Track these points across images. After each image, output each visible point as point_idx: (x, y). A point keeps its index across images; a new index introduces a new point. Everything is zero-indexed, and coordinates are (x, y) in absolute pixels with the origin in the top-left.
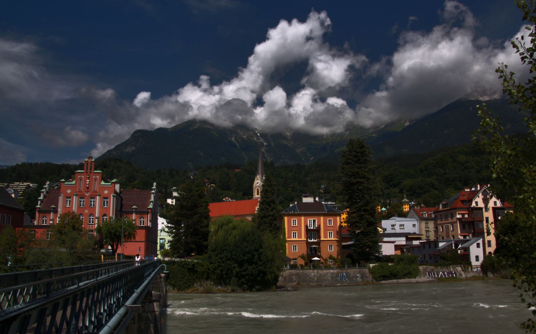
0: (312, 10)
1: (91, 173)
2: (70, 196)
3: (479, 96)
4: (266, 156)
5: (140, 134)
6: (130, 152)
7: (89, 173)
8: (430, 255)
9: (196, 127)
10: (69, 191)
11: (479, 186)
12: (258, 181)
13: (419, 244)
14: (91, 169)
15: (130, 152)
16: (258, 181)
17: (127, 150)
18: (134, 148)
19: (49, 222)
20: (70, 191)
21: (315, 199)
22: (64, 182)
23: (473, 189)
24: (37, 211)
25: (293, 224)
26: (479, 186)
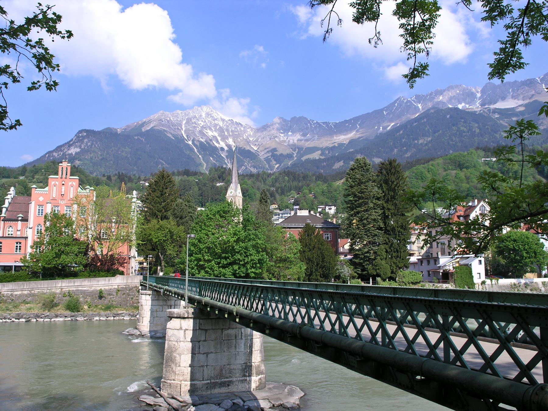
0: (519, 98)
1: (66, 178)
2: (42, 204)
3: (457, 104)
4: (226, 161)
5: (85, 134)
6: (74, 154)
7: (64, 179)
8: (429, 272)
9: (148, 128)
10: (41, 199)
11: (476, 201)
12: (232, 191)
13: (417, 260)
14: (67, 174)
15: (74, 154)
16: (232, 191)
17: (70, 152)
18: (78, 150)
19: (16, 233)
20: (43, 199)
21: (310, 212)
22: (36, 188)
23: (470, 204)
24: (1, 220)
25: (16, 251)
26: (476, 201)
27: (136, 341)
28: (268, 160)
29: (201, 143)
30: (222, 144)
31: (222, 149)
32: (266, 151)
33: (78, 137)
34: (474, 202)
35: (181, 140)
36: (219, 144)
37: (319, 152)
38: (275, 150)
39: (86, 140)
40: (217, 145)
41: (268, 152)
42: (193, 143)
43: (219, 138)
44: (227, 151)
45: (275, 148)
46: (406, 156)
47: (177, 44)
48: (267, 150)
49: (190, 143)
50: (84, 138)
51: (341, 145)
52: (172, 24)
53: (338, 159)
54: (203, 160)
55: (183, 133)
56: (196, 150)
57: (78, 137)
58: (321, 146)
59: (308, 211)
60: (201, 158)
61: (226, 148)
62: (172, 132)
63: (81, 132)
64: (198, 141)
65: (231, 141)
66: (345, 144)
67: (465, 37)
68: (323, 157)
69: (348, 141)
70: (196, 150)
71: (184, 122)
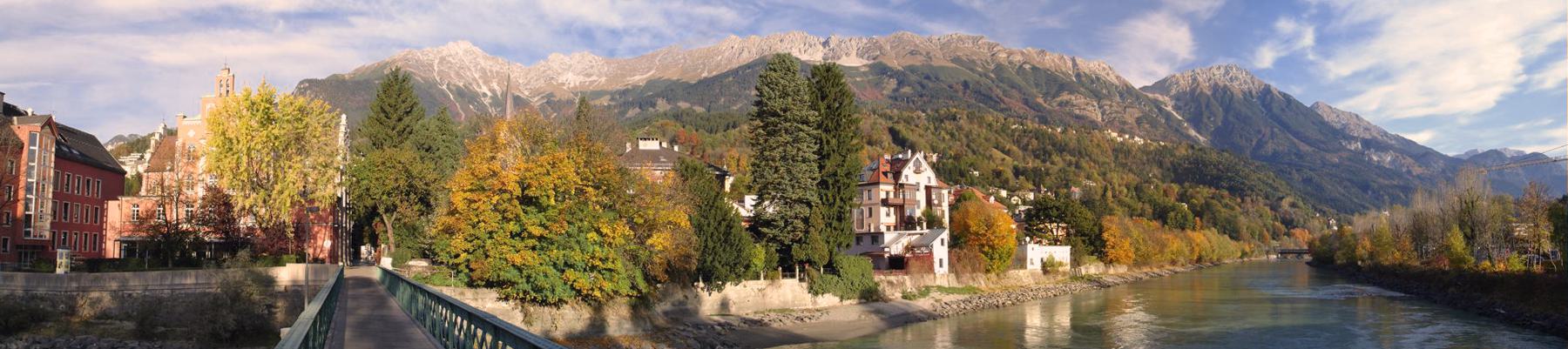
26: (910, 151)
27: (993, 76)
28: (542, 108)
29: (458, 88)
30: (485, 89)
31: (485, 95)
32: (539, 97)
33: (300, 89)
34: (906, 153)
35: (434, 84)
36: (481, 88)
37: (608, 97)
38: (551, 95)
39: (308, 92)
40: (478, 90)
41: (542, 97)
42: (448, 88)
43: (481, 82)
44: (491, 97)
45: (552, 93)
46: (735, 108)
47: (1271, 67)
48: (543, 95)
49: (444, 87)
50: (306, 89)
51: (635, 87)
52: (1492, 150)
53: (632, 104)
54: (462, 108)
55: (435, 74)
56: (451, 96)
57: (300, 89)
58: (610, 88)
59: (658, 142)
60: (459, 107)
61: (489, 94)
62: (421, 74)
63: (301, 83)
64: (455, 85)
65: (495, 85)
66: (641, 86)
67: (719, 303)
68: (613, 103)
69: (645, 82)
70: (451, 96)
71: (437, 61)
